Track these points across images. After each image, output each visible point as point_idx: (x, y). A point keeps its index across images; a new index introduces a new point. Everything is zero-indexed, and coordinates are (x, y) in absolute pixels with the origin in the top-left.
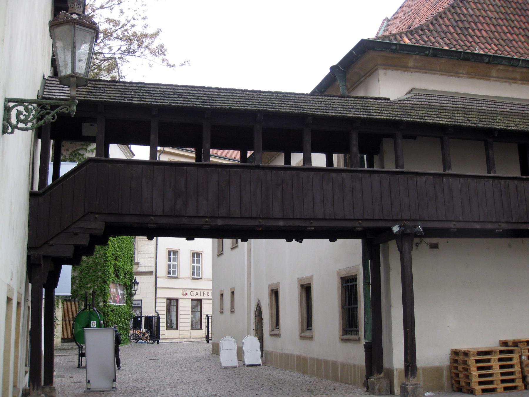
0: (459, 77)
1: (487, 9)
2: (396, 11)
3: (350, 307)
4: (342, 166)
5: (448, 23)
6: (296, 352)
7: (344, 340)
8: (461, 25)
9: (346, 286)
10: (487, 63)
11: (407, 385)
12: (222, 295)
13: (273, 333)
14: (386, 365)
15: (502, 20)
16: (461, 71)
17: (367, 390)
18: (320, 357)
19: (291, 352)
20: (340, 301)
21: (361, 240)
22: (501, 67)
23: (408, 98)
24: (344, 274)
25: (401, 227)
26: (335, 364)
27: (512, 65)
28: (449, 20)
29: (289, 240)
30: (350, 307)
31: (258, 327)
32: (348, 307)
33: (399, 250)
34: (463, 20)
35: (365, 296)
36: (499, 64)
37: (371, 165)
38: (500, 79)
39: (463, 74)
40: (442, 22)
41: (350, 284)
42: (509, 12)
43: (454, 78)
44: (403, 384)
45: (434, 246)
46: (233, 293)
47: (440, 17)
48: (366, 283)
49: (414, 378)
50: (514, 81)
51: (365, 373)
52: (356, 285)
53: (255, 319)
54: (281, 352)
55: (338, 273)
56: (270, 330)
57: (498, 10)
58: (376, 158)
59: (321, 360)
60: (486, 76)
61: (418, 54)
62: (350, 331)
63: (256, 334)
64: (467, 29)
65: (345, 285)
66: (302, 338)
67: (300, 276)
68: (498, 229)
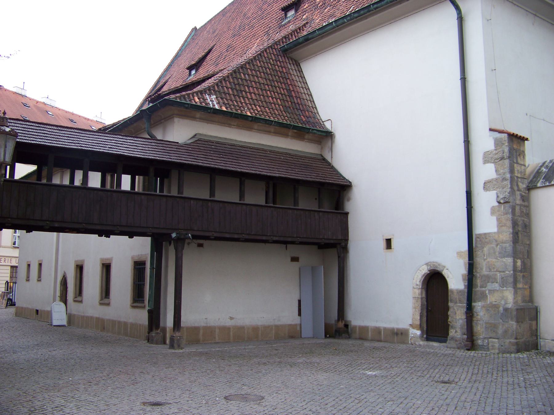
0: (230, 127)
1: (259, 75)
2: (204, 24)
3: (139, 283)
4: (141, 191)
5: (229, 86)
6: (96, 315)
7: (133, 307)
8: (238, 88)
9: (137, 268)
10: (251, 121)
11: (174, 337)
12: (29, 265)
13: (76, 299)
14: (162, 324)
15: (268, 86)
16: (233, 124)
17: (148, 342)
18: (115, 319)
19: (91, 315)
20: (133, 278)
21: (150, 238)
22: (261, 124)
23: (192, 143)
24: (136, 259)
25: (177, 234)
26: (125, 324)
27: (268, 124)
28: (230, 83)
29: (100, 235)
30: (139, 283)
31: (62, 294)
32: (138, 283)
33: (175, 249)
34: (240, 84)
35: (150, 277)
36: (258, 122)
37: (162, 190)
38: (259, 131)
39: (234, 126)
40: (224, 85)
41: (140, 267)
42: (275, 79)
43: (227, 128)
44: (171, 336)
45: (200, 245)
46: (40, 265)
47: (224, 80)
48: (152, 268)
49: (179, 332)
50: (269, 133)
51: (147, 330)
52: (145, 268)
53: (60, 288)
54: (82, 314)
55: (132, 258)
56: (74, 297)
57: (267, 77)
58: (166, 181)
59: (115, 321)
60: (250, 129)
61: (203, 111)
62: (138, 300)
63: (60, 299)
64: (241, 91)
65: (136, 267)
66: (101, 304)
67: (102, 257)
68: (242, 238)
